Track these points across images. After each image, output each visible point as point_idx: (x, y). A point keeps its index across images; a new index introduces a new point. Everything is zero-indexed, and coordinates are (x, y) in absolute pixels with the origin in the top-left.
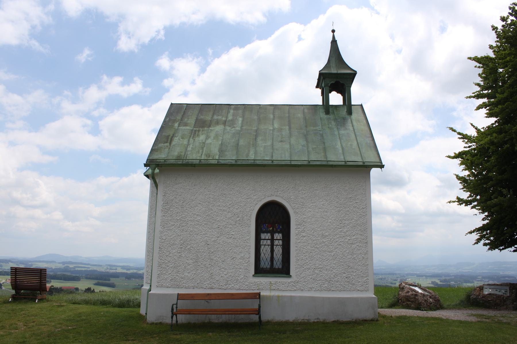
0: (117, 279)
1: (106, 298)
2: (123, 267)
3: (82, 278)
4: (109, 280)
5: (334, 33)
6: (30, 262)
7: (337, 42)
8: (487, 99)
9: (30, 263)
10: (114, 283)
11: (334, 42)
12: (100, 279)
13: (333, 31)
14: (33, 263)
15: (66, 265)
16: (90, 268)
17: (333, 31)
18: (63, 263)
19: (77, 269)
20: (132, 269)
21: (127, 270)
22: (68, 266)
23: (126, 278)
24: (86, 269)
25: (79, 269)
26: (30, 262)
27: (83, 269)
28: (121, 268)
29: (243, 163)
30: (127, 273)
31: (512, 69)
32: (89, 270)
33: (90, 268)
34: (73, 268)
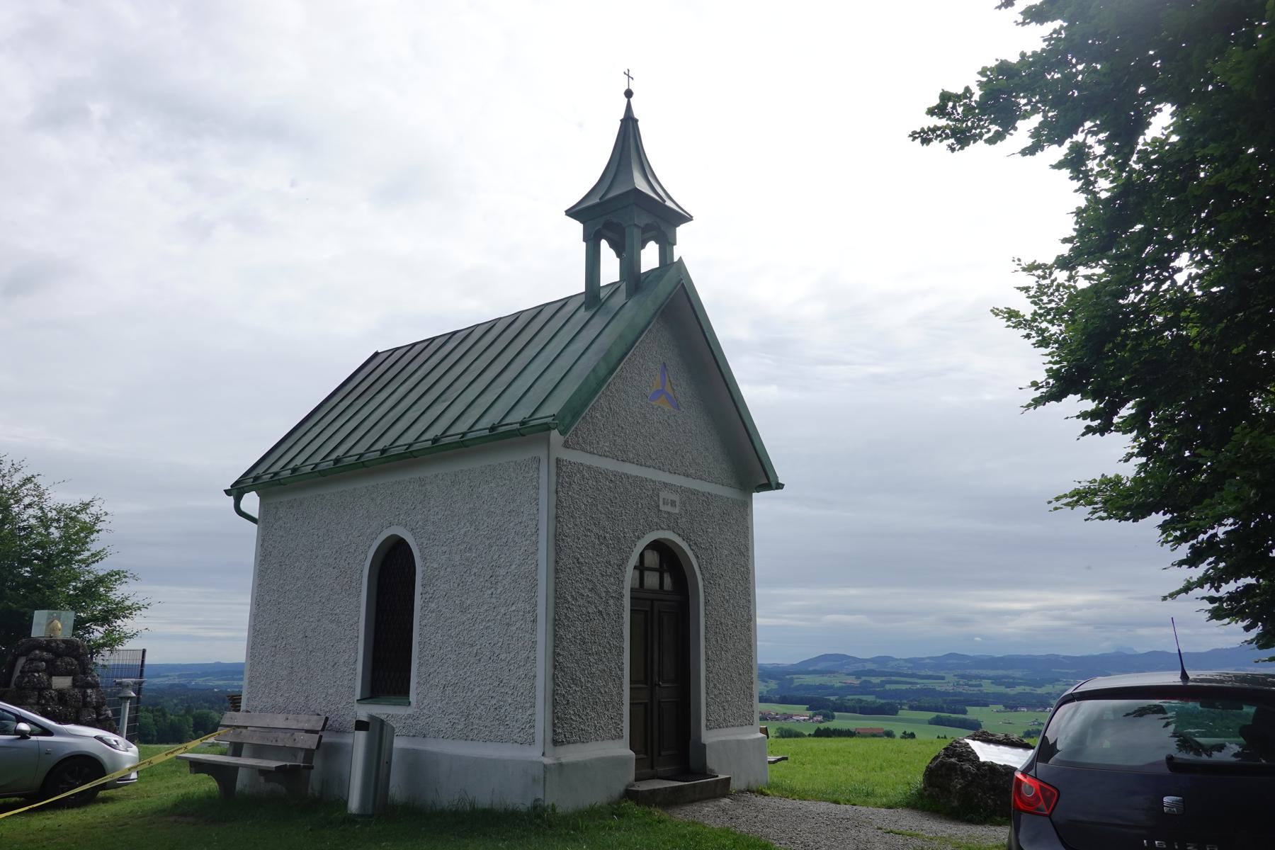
0: (984, 709)
1: (875, 732)
2: (873, 660)
3: (902, 709)
4: (965, 712)
5: (631, 99)
6: (788, 674)
7: (639, 123)
8: (1070, 173)
9: (788, 677)
10: (977, 720)
11: (629, 126)
12: (941, 710)
13: (629, 94)
14: (795, 676)
15: (864, 678)
16: (917, 683)
17: (629, 94)
18: (858, 674)
19: (888, 687)
20: (1020, 684)
21: (1006, 687)
22: (869, 682)
23: (1006, 707)
24: (908, 686)
25: (893, 687)
26: (789, 673)
27: (904, 687)
28: (992, 683)
29: (481, 435)
30: (1005, 695)
31: (1156, 51)
32: (915, 688)
33: (917, 683)
34: (878, 683)
